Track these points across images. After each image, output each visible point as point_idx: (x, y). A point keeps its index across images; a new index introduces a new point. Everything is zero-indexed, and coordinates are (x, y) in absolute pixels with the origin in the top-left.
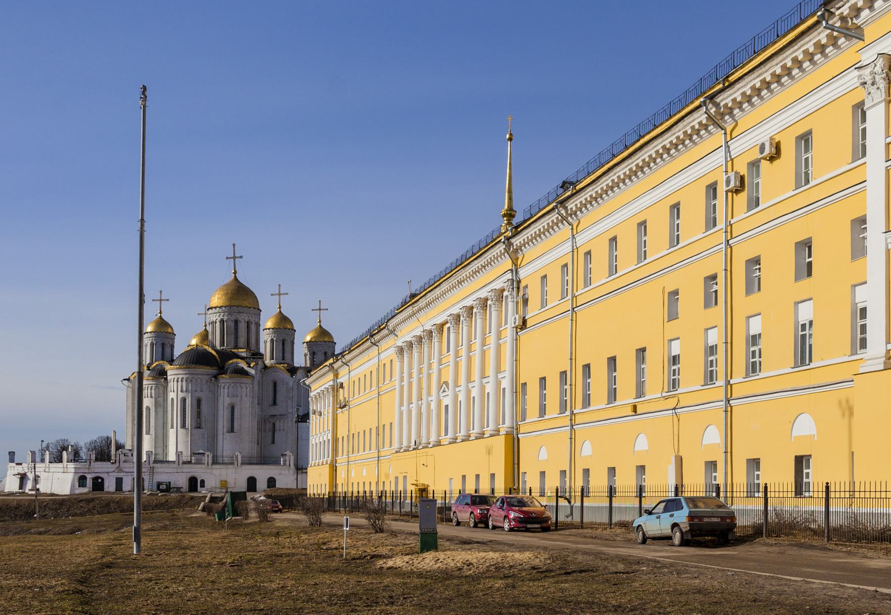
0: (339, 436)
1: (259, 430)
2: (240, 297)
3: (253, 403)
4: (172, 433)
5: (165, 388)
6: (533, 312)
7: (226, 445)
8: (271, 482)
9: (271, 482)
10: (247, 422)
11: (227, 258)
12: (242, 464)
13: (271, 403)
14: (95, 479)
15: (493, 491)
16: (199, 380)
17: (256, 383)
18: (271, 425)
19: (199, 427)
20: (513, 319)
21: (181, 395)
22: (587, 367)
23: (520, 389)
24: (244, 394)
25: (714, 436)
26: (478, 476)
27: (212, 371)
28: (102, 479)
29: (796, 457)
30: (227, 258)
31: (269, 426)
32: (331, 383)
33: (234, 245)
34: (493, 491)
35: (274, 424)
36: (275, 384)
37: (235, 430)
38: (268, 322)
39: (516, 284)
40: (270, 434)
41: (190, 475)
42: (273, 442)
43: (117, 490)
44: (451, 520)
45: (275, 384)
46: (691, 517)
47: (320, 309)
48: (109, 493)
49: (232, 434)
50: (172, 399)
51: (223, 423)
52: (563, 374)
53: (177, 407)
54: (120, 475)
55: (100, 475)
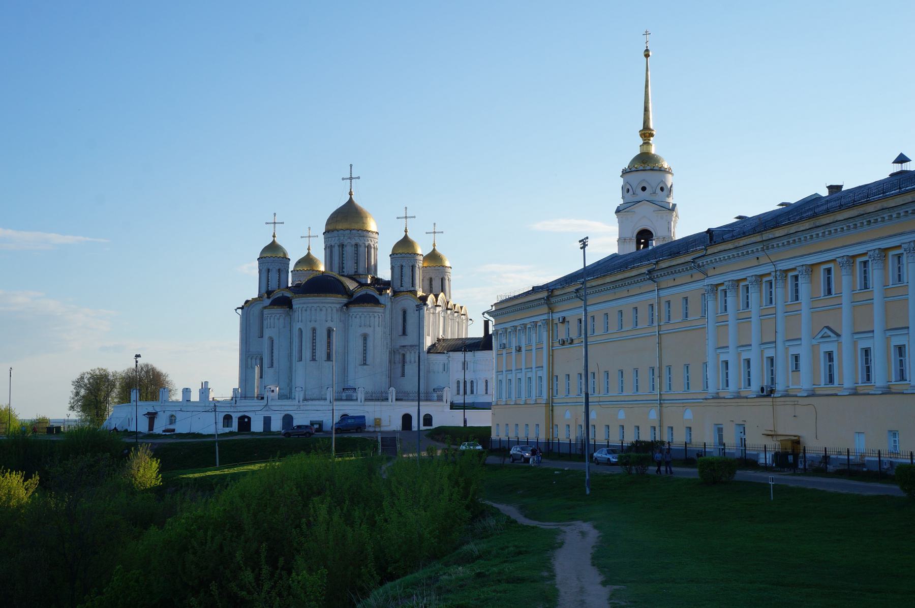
0: (559, 371)
1: (390, 362)
2: (347, 221)
3: (385, 333)
8: (428, 420)
10: (379, 353)
11: (343, 179)
12: (366, 400)
13: (401, 333)
14: (241, 419)
15: (465, 421)
16: (329, 310)
17: (388, 312)
18: (401, 357)
24: (377, 323)
25: (653, 415)
27: (345, 300)
28: (249, 419)
30: (343, 179)
31: (398, 357)
32: (545, 317)
33: (351, 166)
34: (465, 421)
35: (404, 355)
36: (405, 312)
40: (400, 365)
41: (403, 413)
42: (403, 375)
47: (275, 223)
48: (254, 433)
49: (365, 367)
50: (301, 330)
53: (307, 336)
54: (267, 414)
55: (246, 414)
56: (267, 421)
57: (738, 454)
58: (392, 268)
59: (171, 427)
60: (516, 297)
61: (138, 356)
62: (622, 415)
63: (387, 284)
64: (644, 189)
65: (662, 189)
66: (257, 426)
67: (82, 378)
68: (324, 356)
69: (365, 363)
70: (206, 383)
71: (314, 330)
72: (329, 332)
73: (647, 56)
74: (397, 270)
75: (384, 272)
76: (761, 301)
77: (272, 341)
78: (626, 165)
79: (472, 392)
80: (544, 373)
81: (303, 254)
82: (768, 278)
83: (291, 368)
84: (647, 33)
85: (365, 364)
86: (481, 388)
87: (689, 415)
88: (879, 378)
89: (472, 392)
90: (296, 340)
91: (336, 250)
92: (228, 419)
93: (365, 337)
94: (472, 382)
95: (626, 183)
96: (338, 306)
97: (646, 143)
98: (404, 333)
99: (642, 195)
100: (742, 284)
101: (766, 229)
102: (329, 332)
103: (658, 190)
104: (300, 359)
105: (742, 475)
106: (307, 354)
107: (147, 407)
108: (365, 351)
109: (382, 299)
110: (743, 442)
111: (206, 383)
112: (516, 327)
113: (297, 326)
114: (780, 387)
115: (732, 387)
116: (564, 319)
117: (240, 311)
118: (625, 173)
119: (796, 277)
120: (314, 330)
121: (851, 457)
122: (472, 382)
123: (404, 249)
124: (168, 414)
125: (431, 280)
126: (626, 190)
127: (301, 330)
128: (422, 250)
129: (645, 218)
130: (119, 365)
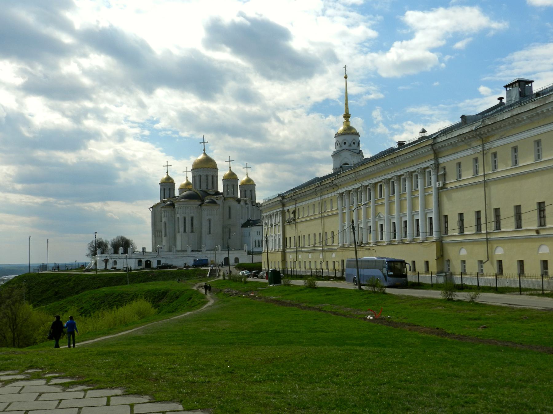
0: (288, 236)
4: (178, 237)
5: (175, 214)
6: (452, 182)
7: (208, 241)
8: (237, 260)
9: (237, 260)
10: (217, 229)
14: (146, 262)
19: (192, 232)
20: (435, 184)
21: (183, 215)
22: (304, 236)
23: (443, 219)
26: (309, 235)
27: (199, 203)
28: (150, 262)
29: (515, 206)
31: (227, 230)
32: (281, 209)
35: (230, 229)
36: (230, 208)
37: (211, 232)
38: (221, 174)
39: (437, 166)
43: (425, 272)
44: (241, 281)
45: (230, 208)
46: (281, 283)
50: (178, 218)
51: (205, 229)
52: (320, 234)
53: (181, 221)
58: (223, 186)
59: (115, 266)
60: (270, 200)
61: (96, 233)
62: (310, 256)
63: (221, 194)
64: (345, 143)
66: (154, 264)
67: (92, 243)
68: (190, 230)
69: (210, 233)
71: (185, 218)
72: (192, 218)
73: (346, 77)
74: (226, 187)
75: (221, 189)
76: (412, 187)
77: (165, 224)
80: (281, 237)
83: (175, 235)
84: (345, 67)
85: (210, 233)
87: (334, 255)
90: (177, 222)
91: (197, 178)
92: (140, 262)
93: (210, 221)
96: (196, 206)
97: (347, 121)
98: (230, 217)
99: (344, 147)
100: (402, 177)
101: (310, 307)
102: (192, 218)
103: (352, 144)
104: (179, 232)
105: (320, 284)
106: (182, 229)
108: (210, 227)
109: (218, 202)
113: (178, 216)
117: (151, 209)
120: (185, 218)
123: (231, 178)
125: (245, 191)
127: (178, 218)
128: (242, 178)
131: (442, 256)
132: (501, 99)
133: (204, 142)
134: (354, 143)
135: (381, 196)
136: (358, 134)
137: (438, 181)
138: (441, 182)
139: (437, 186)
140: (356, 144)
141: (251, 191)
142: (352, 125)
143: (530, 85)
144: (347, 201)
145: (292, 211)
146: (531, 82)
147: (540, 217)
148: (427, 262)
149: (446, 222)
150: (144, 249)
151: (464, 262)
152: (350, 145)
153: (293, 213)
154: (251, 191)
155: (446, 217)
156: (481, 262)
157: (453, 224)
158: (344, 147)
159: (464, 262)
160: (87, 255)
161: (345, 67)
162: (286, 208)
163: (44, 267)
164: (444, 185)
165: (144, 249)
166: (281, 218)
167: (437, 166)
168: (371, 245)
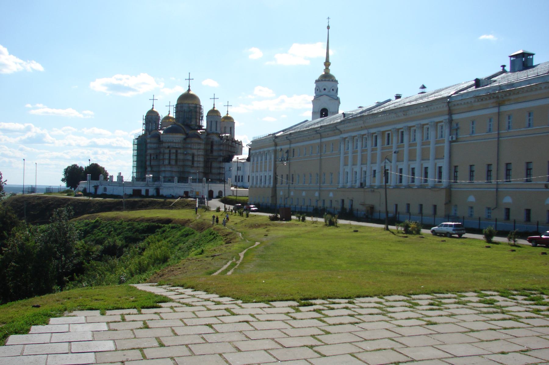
23: (453, 169)
25: (317, 194)
54: (148, 188)
56: (147, 191)
57: (378, 218)
59: (105, 193)
65: (333, 90)
70: (120, 173)
74: (209, 123)
78: (317, 78)
79: (242, 181)
80: (272, 174)
81: (211, 108)
82: (414, 128)
84: (328, 18)
86: (246, 179)
88: (404, 182)
89: (242, 181)
94: (242, 176)
95: (317, 86)
99: (324, 92)
103: (331, 90)
107: (95, 183)
110: (455, 213)
111: (120, 173)
112: (264, 152)
114: (368, 184)
115: (417, 183)
116: (281, 149)
118: (317, 81)
119: (415, 130)
121: (539, 226)
122: (242, 176)
123: (213, 113)
124: (103, 186)
126: (317, 90)
129: (326, 103)
130: (84, 164)
131: (450, 201)
132: (503, 66)
133: (189, 79)
134: (333, 90)
135: (388, 144)
136: (336, 82)
137: (450, 135)
138: (454, 136)
139: (450, 140)
140: (335, 91)
141: (231, 128)
142: (332, 72)
143: (531, 57)
144: (350, 145)
145: (285, 151)
146: (533, 55)
147: (471, 176)
148: (435, 206)
149: (456, 172)
150: (120, 177)
151: (472, 208)
152: (329, 91)
153: (287, 152)
154: (231, 128)
155: (456, 167)
156: (489, 209)
157: (463, 172)
158: (324, 92)
159: (472, 208)
160: (63, 180)
161: (328, 18)
162: (278, 148)
163: (33, 189)
164: (457, 138)
165: (120, 177)
166: (273, 156)
167: (451, 121)
168: (376, 187)
